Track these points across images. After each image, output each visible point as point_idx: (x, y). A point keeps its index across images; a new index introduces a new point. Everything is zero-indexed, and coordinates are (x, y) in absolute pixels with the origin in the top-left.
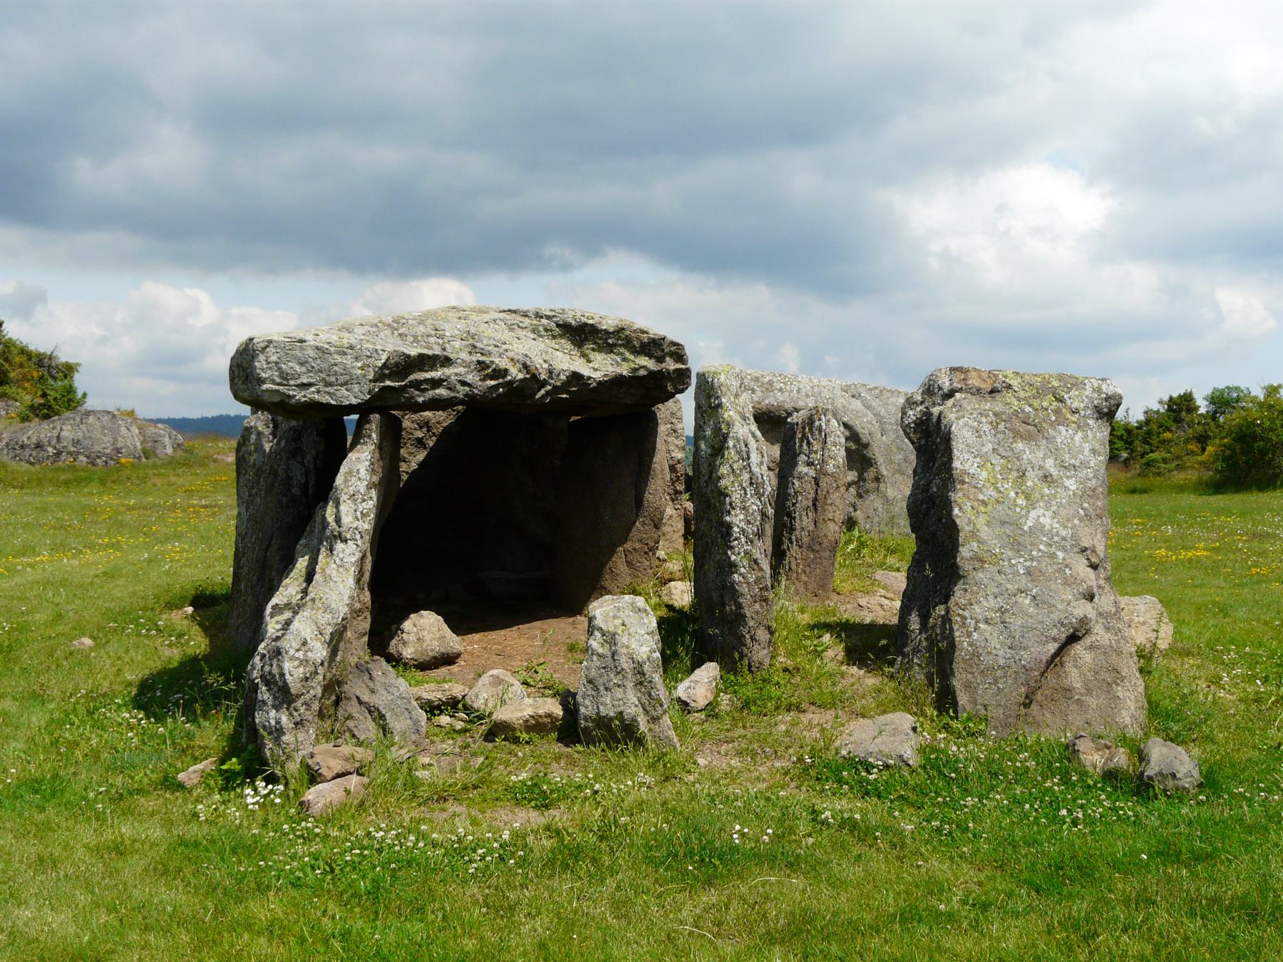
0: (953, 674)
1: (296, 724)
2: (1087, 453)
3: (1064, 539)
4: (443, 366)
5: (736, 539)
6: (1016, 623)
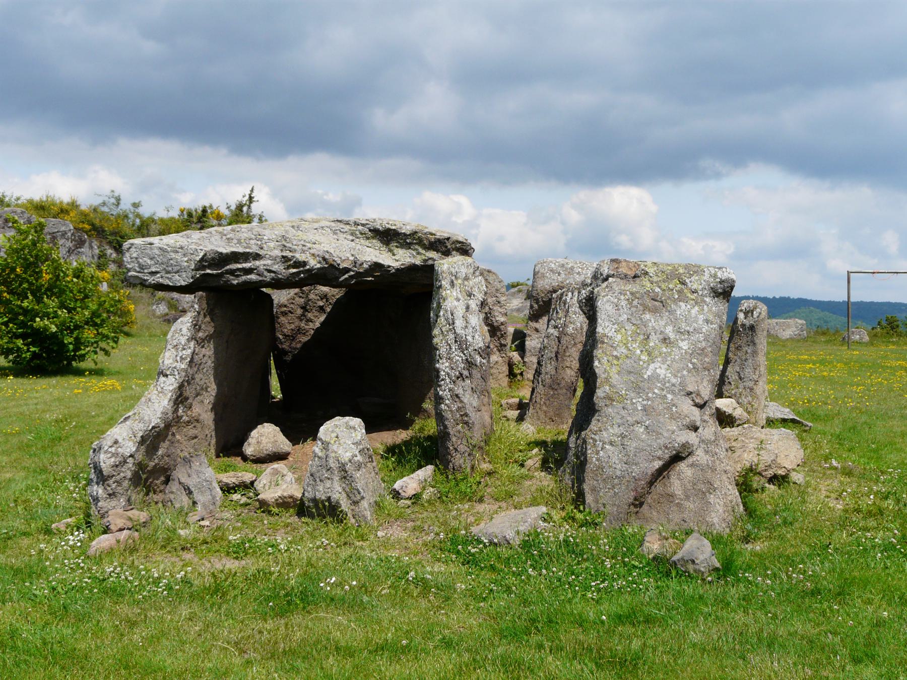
0: (584, 481)
1: (110, 495)
2: (700, 322)
3: (673, 385)
4: (255, 259)
5: (443, 380)
6: (632, 445)
